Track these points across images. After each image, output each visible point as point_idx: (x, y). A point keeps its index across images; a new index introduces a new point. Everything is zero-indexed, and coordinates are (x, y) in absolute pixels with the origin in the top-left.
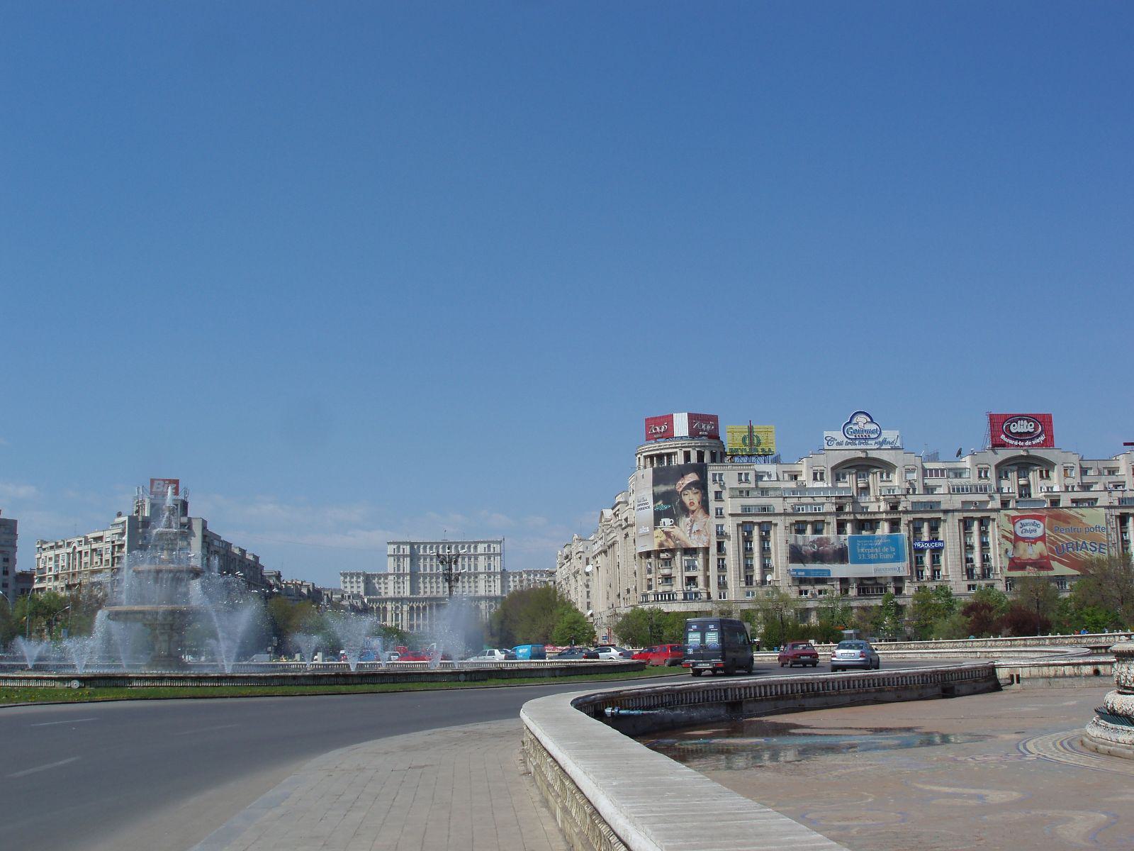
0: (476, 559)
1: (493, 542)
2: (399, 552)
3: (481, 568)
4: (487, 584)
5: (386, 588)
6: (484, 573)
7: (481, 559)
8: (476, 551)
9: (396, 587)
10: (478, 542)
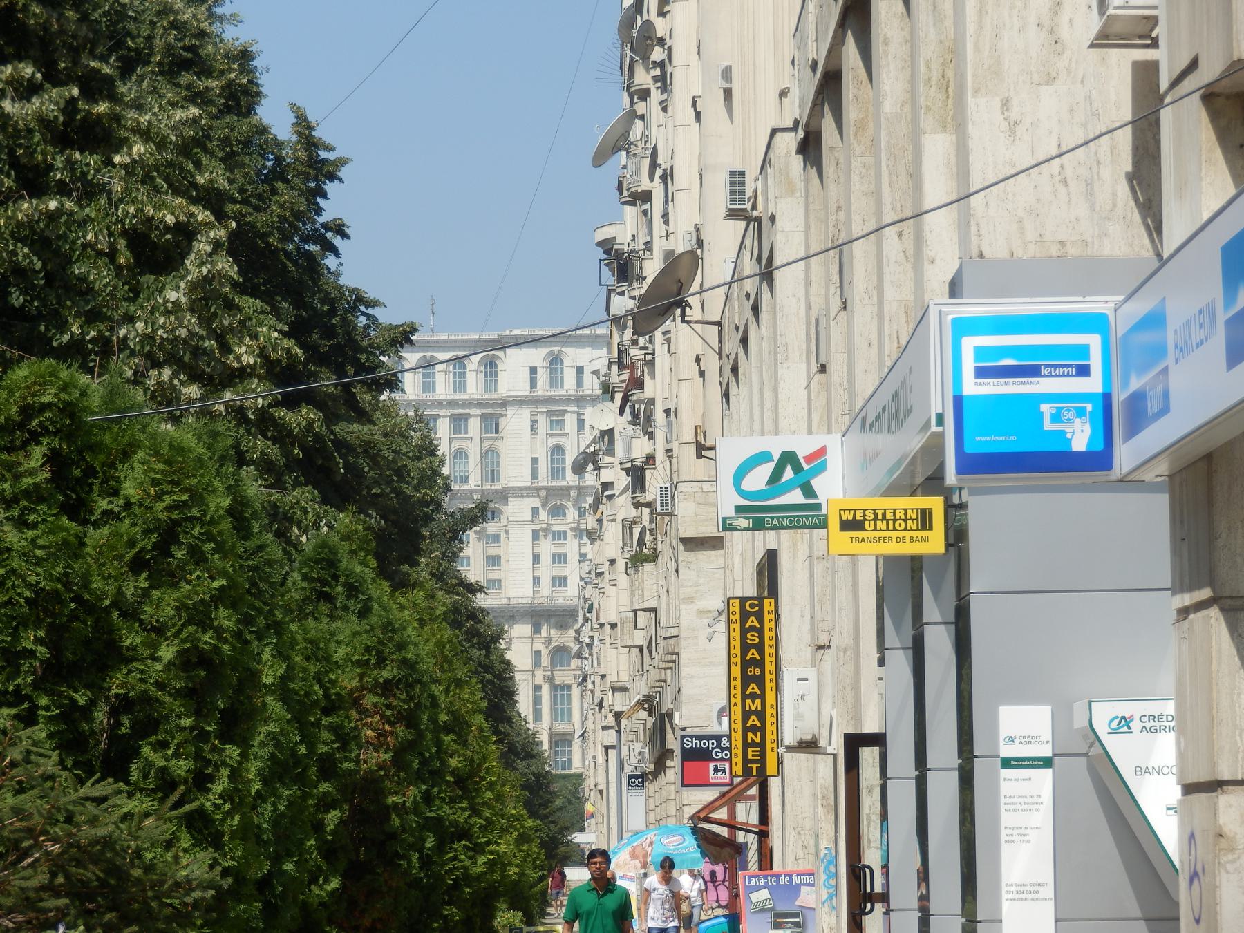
0: (492, 424)
2: (557, 381)
3: (515, 472)
4: (546, 548)
6: (532, 491)
7: (516, 421)
9: (545, 559)
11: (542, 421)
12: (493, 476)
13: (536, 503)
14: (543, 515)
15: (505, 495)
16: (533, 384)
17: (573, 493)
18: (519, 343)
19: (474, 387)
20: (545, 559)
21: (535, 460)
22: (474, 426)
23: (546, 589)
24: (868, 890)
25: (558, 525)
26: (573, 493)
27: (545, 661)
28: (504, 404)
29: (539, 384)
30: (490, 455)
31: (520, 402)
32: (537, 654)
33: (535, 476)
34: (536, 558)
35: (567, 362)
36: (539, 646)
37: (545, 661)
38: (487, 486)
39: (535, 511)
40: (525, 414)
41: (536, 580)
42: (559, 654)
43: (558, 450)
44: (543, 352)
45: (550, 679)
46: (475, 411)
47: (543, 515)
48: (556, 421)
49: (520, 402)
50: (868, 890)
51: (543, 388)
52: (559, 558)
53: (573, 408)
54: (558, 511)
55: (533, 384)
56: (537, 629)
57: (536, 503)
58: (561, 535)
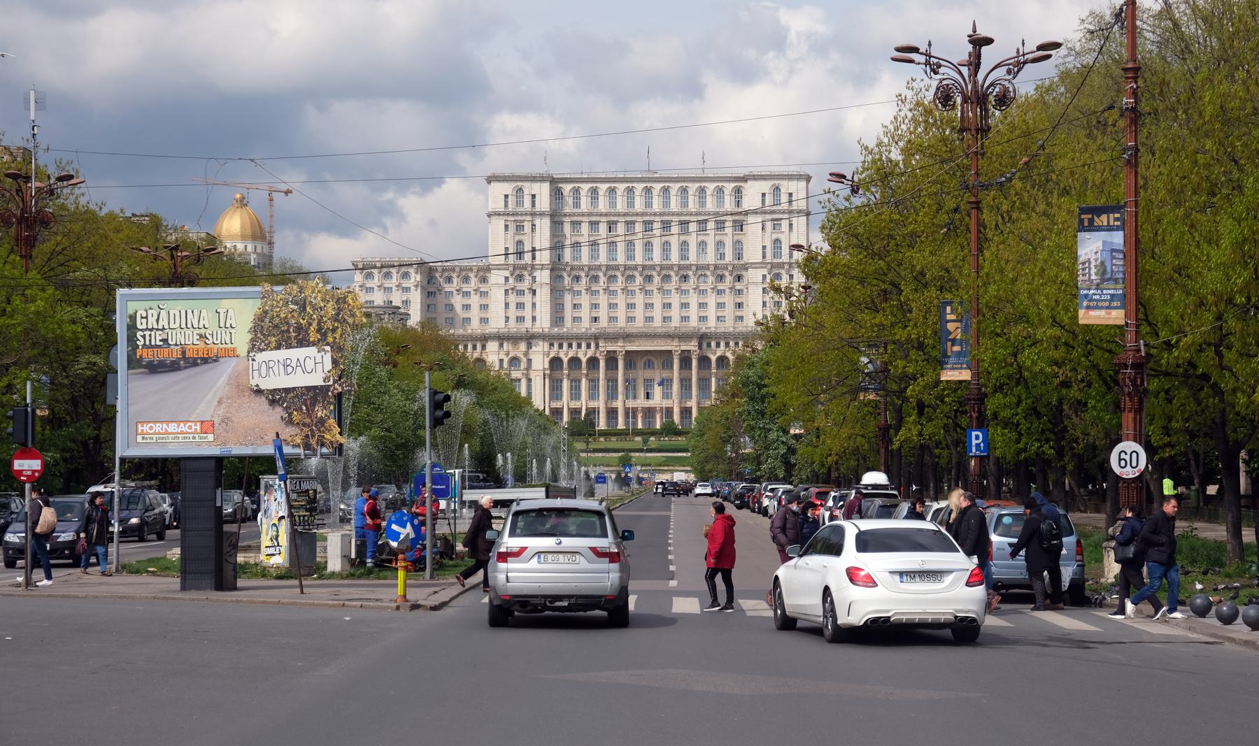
0: (739, 226)
1: (790, 177)
2: (519, 203)
3: (752, 254)
4: (513, 299)
5: (484, 307)
6: (762, 265)
8: (738, 204)
9: (512, 306)
10: (744, 179)
11: (769, 225)
12: (739, 256)
14: (511, 280)
15: (746, 267)
16: (763, 201)
17: (786, 267)
20: (512, 306)
21: (764, 247)
23: (512, 322)
24: (52, 562)
25: (520, 286)
28: (746, 213)
31: (755, 212)
32: (501, 361)
33: (764, 257)
34: (507, 305)
35: (526, 192)
36: (502, 356)
37: (505, 366)
38: (736, 262)
39: (507, 279)
40: (759, 218)
41: (507, 318)
43: (777, 241)
47: (511, 280)
48: (776, 224)
49: (755, 212)
50: (52, 562)
52: (520, 306)
54: (520, 278)
55: (506, 205)
56: (501, 345)
57: (507, 273)
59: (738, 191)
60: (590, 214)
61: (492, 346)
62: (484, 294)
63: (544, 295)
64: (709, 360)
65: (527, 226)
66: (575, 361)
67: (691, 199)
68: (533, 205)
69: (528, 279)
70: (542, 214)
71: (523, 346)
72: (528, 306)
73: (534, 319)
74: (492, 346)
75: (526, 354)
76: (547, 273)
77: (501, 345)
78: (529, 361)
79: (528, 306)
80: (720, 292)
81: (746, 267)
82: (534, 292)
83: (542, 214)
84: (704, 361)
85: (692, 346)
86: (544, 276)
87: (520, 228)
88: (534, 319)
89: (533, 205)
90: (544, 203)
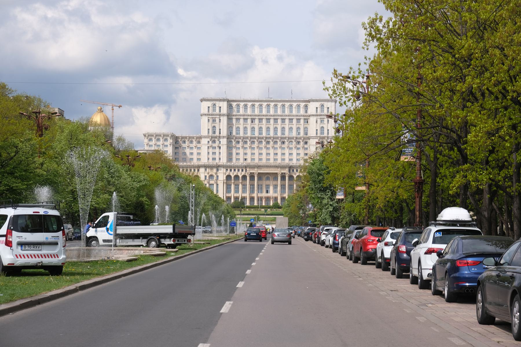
0: (306, 121)
2: (214, 110)
3: (312, 132)
5: (199, 154)
7: (312, 120)
9: (211, 153)
11: (319, 121)
12: (306, 134)
13: (209, 140)
14: (210, 142)
15: (309, 138)
17: (326, 138)
18: (313, 101)
19: (302, 112)
20: (211, 153)
22: (302, 121)
25: (214, 145)
26: (326, 138)
27: (207, 178)
29: (318, 111)
30: (306, 129)
31: (313, 115)
32: (206, 176)
34: (208, 153)
36: (206, 174)
37: (207, 178)
38: (305, 136)
39: (208, 142)
41: (208, 159)
42: (211, 176)
44: (320, 103)
45: (209, 182)
46: (302, 118)
47: (210, 142)
49: (313, 115)
51: (319, 112)
52: (214, 153)
53: (218, 117)
54: (214, 142)
56: (206, 170)
57: (209, 140)
58: (291, 148)
59: (306, 106)
60: (267, 116)
61: (202, 170)
62: (199, 148)
63: (224, 149)
64: (293, 177)
65: (217, 120)
66: (237, 177)
67: (286, 109)
68: (220, 111)
69: (217, 142)
70: (223, 115)
71: (215, 170)
72: (217, 153)
73: (220, 159)
74: (202, 170)
75: (216, 173)
76: (225, 140)
77: (206, 170)
78: (218, 176)
79: (217, 153)
80: (268, 148)
81: (200, 138)
82: (220, 148)
83: (223, 115)
84: (291, 177)
85: (286, 171)
86: (224, 141)
87: (214, 121)
88: (220, 159)
89: (220, 111)
90: (224, 110)
